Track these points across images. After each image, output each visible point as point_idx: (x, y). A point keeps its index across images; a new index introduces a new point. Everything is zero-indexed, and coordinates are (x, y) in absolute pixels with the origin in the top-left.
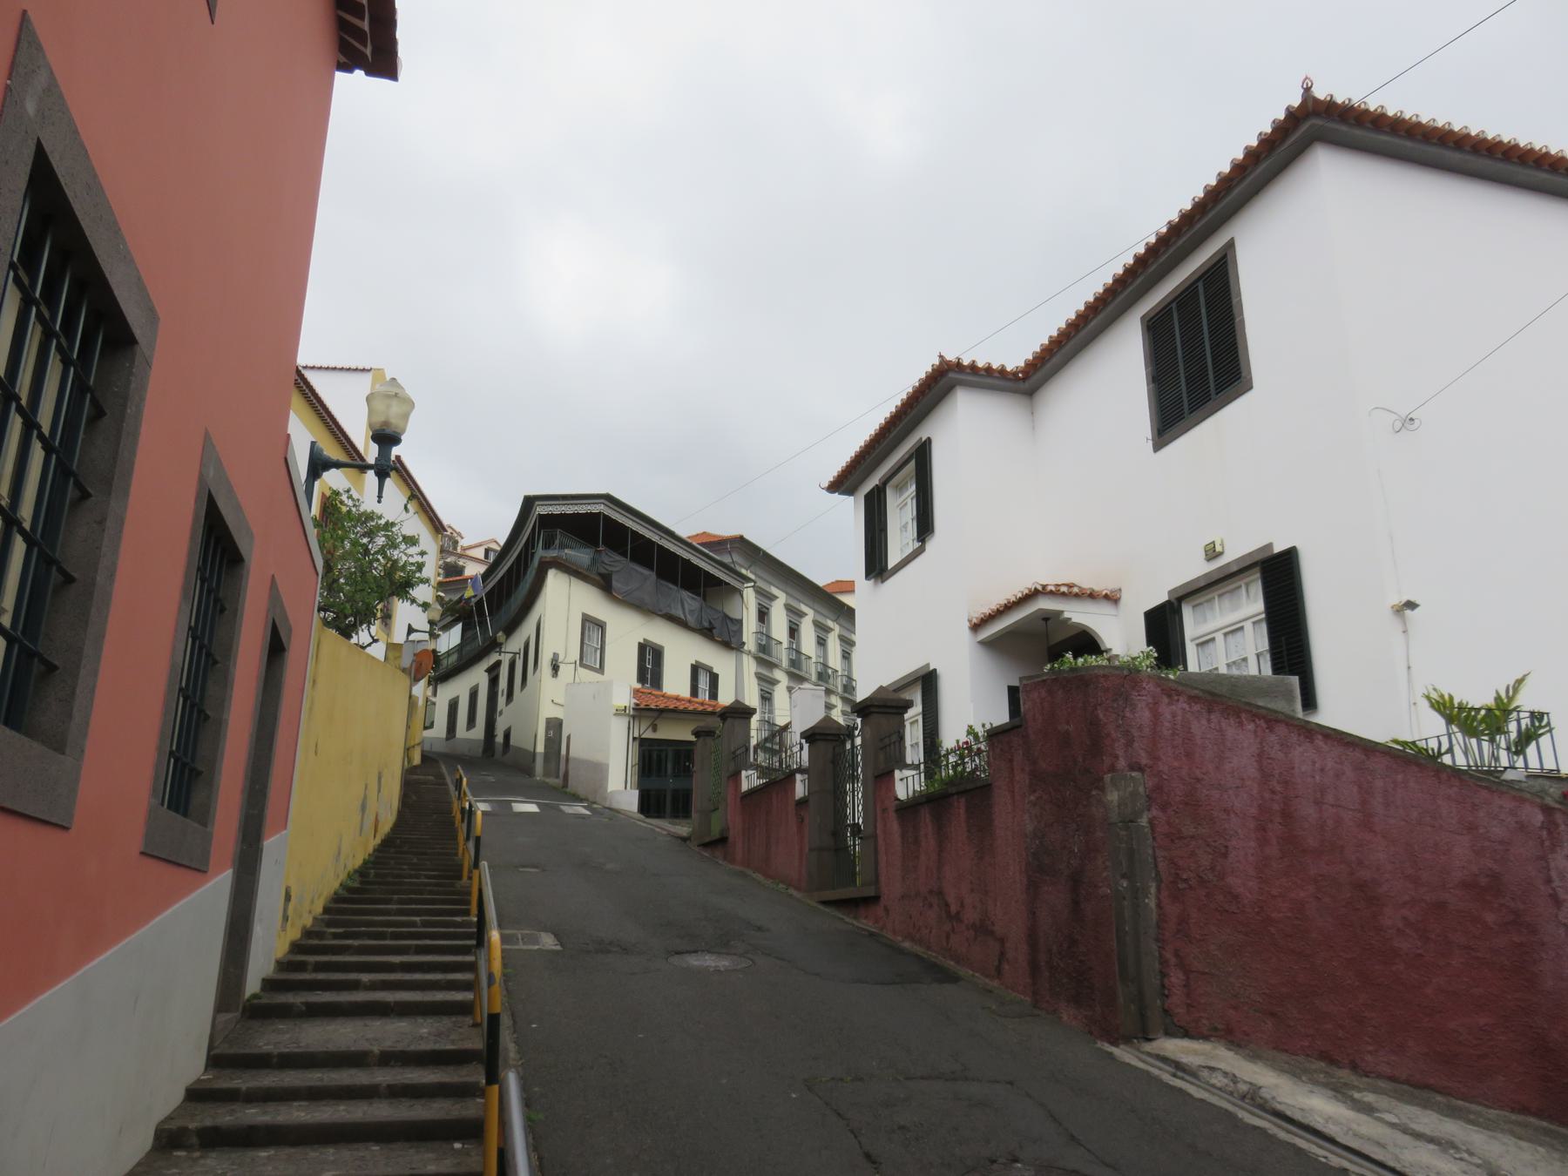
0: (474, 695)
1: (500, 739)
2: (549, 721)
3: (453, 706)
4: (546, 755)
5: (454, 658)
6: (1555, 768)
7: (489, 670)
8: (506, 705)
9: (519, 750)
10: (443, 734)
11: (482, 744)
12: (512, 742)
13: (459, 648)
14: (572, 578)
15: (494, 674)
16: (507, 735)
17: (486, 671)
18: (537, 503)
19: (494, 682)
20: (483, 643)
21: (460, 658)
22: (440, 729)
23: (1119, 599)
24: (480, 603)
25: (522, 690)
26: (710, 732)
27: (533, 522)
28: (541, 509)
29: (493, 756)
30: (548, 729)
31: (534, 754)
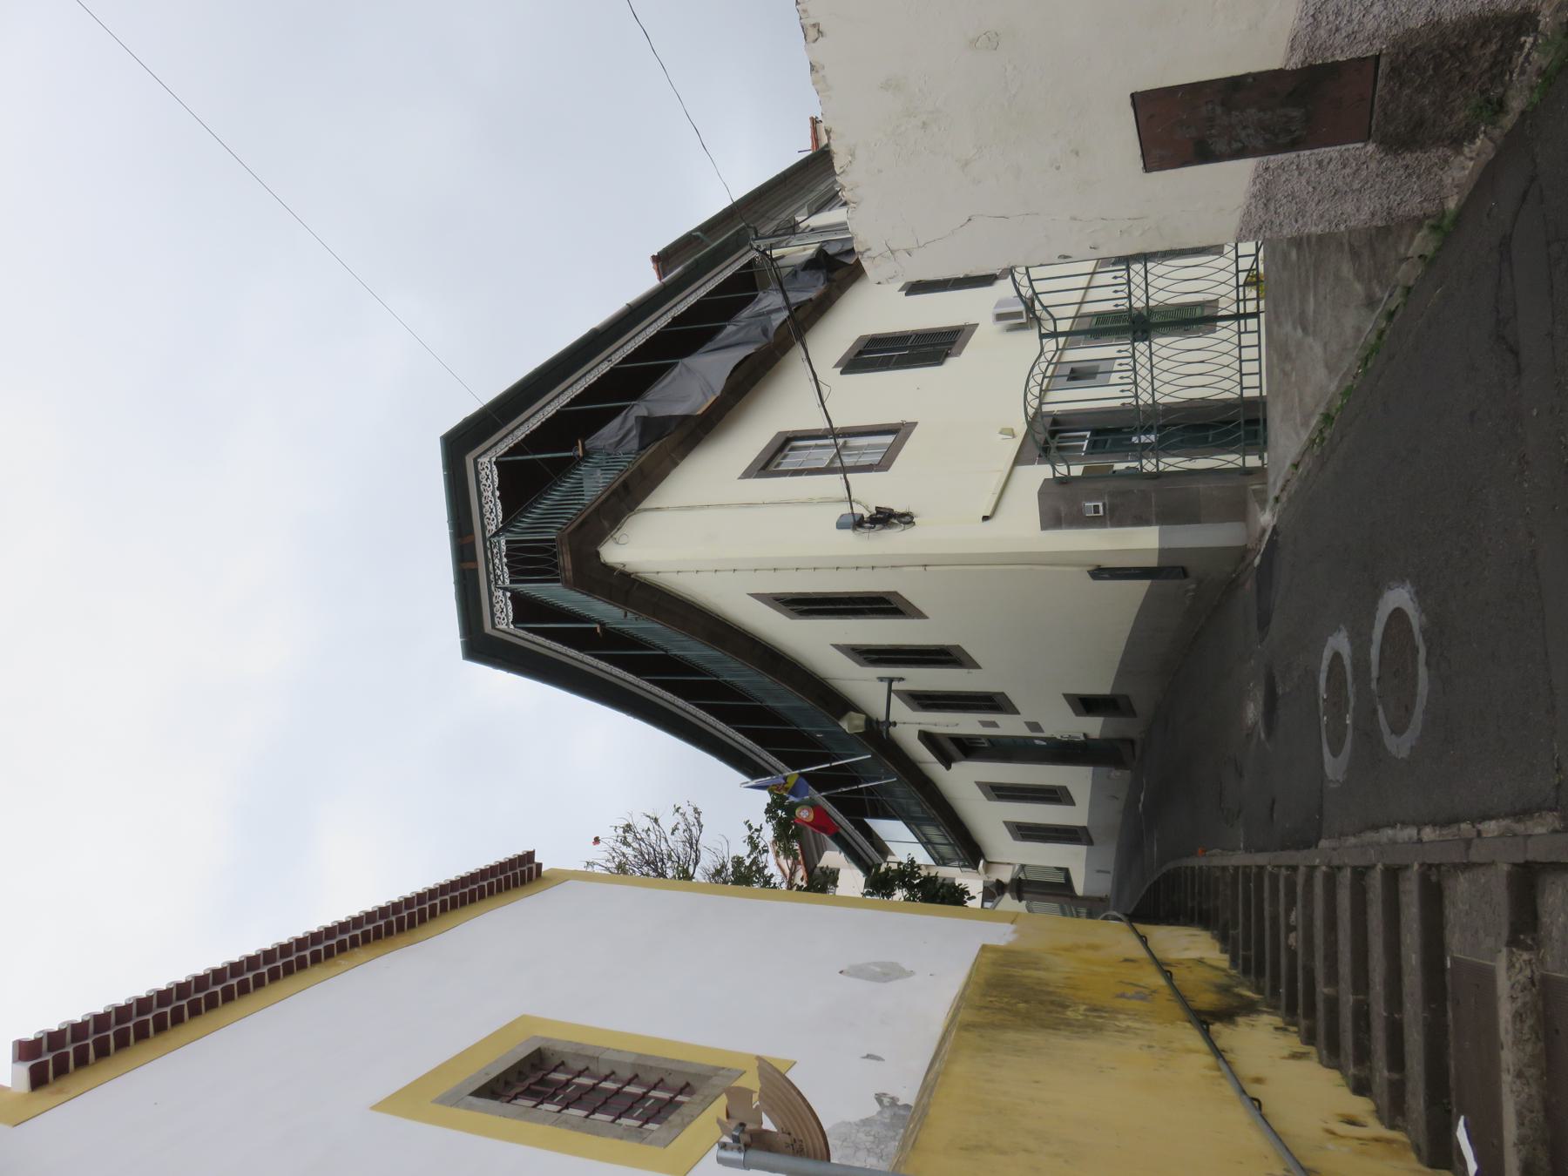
1: (1093, 726)
2: (1053, 518)
3: (1025, 832)
4: (1167, 516)
5: (933, 832)
6: (1225, 1035)
7: (947, 761)
8: (1018, 713)
9: (1127, 668)
10: (1080, 850)
11: (1103, 770)
12: (1101, 686)
13: (912, 822)
14: (645, 504)
16: (1086, 705)
17: (948, 767)
18: (488, 628)
19: (968, 748)
21: (930, 821)
23: (1392, 589)
25: (917, 614)
27: (530, 636)
28: (502, 618)
29: (1132, 742)
30: (1079, 520)
31: (1164, 571)
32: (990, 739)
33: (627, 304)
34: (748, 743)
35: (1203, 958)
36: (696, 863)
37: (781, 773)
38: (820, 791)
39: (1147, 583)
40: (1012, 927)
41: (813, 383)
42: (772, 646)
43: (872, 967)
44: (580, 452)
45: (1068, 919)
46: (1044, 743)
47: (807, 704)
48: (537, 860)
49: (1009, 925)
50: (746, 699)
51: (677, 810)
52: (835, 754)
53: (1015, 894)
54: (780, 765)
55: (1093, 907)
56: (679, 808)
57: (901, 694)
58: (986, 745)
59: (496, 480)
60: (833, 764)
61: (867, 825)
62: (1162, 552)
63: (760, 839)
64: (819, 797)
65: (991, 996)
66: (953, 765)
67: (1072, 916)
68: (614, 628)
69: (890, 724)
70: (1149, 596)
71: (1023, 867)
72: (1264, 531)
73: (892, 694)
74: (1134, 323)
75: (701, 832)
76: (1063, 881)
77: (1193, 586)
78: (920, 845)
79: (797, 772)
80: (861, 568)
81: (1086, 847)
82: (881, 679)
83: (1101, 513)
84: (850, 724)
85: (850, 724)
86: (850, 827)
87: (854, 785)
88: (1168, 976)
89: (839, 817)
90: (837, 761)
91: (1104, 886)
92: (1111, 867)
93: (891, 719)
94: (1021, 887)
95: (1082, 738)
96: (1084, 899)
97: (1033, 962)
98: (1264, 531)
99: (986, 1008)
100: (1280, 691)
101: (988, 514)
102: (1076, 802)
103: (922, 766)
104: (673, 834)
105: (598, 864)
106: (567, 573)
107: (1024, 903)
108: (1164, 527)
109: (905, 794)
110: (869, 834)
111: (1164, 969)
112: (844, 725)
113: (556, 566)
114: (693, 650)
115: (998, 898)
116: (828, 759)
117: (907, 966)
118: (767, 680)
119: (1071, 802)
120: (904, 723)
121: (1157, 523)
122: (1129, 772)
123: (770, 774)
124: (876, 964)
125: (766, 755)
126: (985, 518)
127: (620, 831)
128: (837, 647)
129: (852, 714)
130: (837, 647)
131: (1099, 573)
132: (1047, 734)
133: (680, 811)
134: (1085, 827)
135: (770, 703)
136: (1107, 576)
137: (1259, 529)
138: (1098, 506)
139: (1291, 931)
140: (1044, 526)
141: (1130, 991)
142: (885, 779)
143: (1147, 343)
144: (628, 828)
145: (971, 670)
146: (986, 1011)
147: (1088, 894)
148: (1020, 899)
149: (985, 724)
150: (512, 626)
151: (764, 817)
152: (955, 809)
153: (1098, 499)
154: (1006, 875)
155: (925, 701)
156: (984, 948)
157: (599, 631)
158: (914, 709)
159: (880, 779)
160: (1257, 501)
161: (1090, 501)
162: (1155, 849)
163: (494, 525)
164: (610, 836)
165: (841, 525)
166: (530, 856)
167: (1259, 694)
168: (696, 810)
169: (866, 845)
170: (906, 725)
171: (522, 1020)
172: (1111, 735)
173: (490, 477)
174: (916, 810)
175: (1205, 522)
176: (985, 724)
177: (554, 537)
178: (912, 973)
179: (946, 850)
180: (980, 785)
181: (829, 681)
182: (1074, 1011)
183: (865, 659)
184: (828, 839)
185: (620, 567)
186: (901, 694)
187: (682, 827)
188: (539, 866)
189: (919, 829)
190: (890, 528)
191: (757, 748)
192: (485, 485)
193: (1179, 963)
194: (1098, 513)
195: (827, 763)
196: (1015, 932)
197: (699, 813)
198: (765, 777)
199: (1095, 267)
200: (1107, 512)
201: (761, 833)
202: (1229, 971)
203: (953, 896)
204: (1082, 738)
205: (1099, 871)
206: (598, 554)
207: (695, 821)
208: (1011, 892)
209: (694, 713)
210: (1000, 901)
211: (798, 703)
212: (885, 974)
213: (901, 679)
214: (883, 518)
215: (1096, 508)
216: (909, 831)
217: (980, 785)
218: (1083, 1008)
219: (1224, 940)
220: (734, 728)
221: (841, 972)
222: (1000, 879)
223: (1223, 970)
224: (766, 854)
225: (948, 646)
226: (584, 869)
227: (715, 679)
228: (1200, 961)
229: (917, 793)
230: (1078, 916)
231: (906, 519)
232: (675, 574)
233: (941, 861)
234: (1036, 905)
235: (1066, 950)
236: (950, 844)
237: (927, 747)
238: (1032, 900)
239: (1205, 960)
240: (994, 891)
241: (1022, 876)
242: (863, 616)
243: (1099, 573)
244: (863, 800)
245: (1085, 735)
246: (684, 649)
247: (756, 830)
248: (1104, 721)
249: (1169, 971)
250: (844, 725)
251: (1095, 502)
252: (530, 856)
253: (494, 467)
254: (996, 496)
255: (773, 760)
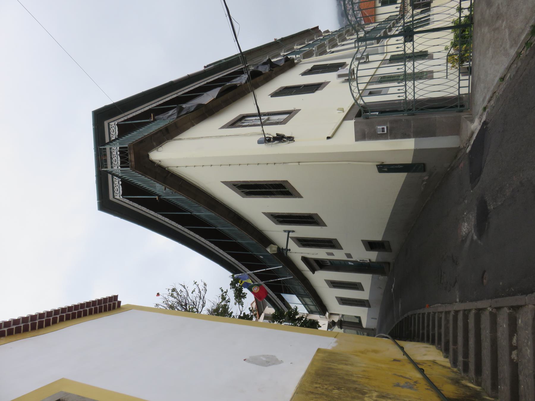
0: (335, 284)
1: (372, 256)
2: (361, 136)
3: (344, 301)
5: (308, 300)
7: (313, 270)
8: (342, 249)
10: (366, 309)
11: (376, 276)
12: (378, 237)
13: (299, 296)
15: (315, 265)
16: (371, 245)
17: (314, 273)
18: (111, 198)
20: (290, 275)
22: (361, 312)
24: (260, 276)
26: (381, 113)
27: (131, 203)
29: (389, 263)
32: (330, 260)
33: (188, 75)
34: (233, 259)
35: (435, 360)
36: (203, 306)
37: (246, 272)
38: (262, 281)
39: (405, 174)
40: (335, 340)
41: (228, 17)
42: (235, 211)
43: (262, 358)
44: (152, 120)
45: (359, 336)
46: (353, 264)
47: (254, 241)
48: (119, 299)
49: (334, 338)
50: (246, 251)
51: (195, 283)
52: (268, 265)
53: (339, 326)
54: (246, 270)
55: (370, 332)
56: (196, 282)
57: (293, 238)
58: (329, 264)
59: (117, 132)
60: (267, 269)
61: (282, 296)
62: (417, 152)
63: (226, 296)
64: (262, 283)
65: (316, 383)
66: (316, 272)
67: (361, 335)
68: (165, 199)
69: (287, 250)
70: (406, 185)
71: (343, 315)
72: (473, 133)
73: (289, 238)
74: (405, 32)
75: (205, 293)
76: (358, 322)
77: (426, 178)
78: (302, 305)
79: (252, 272)
80: (269, 164)
81: (367, 308)
82: (285, 231)
83: (386, 132)
84: (271, 250)
85: (271, 250)
86: (275, 297)
87: (276, 279)
88: (422, 371)
89: (268, 290)
90: (268, 268)
91: (374, 324)
92: (377, 316)
93: (288, 248)
94: (341, 324)
95: (368, 261)
96: (366, 329)
97: (345, 361)
98: (473, 133)
99: (312, 393)
100: (491, 207)
101: (330, 136)
102: (365, 290)
103: (303, 272)
104: (192, 293)
105: (160, 305)
106: (132, 163)
107: (343, 330)
108: (417, 139)
109: (299, 287)
110: (283, 300)
111: (415, 364)
112: (268, 250)
113: (127, 160)
114: (204, 213)
115: (333, 328)
116: (265, 267)
117: (279, 358)
118: (236, 229)
119: (362, 289)
120: (296, 253)
121: (414, 137)
122: (387, 277)
123: (241, 273)
124: (263, 356)
125: (240, 265)
126: (328, 138)
127: (170, 291)
128: (264, 213)
129: (272, 245)
130: (264, 213)
131: (383, 168)
132: (354, 259)
133: (197, 283)
134: (368, 300)
135: (240, 241)
136: (386, 169)
137: (469, 133)
138: (384, 128)
139: (514, 350)
140: (357, 139)
141: (402, 382)
142: (289, 277)
143: (412, 43)
144: (174, 290)
145: (322, 227)
146: (312, 396)
147: (368, 327)
148: (341, 329)
149: (329, 254)
150: (121, 197)
151: (230, 286)
152: (316, 290)
153: (384, 125)
154: (336, 319)
155: (304, 242)
156: (319, 350)
157: (157, 199)
158: (299, 247)
159: (287, 277)
160: (468, 120)
161: (380, 125)
162: (400, 307)
163: (115, 152)
164: (165, 293)
165: (260, 142)
166: (116, 297)
167: (472, 217)
168: (205, 285)
169: (280, 302)
170: (296, 254)
171: (62, 381)
172: (381, 260)
173: (114, 131)
174: (302, 291)
175: (439, 136)
176: (329, 254)
177: (127, 146)
178: (281, 362)
179: (313, 308)
180: (327, 281)
181: (263, 231)
182: (369, 397)
183: (277, 220)
184: (267, 301)
185: (157, 162)
186: (293, 238)
187: (197, 291)
188: (119, 303)
189: (303, 299)
190: (282, 142)
191: (236, 262)
192: (112, 135)
193: (424, 362)
194: (384, 132)
195: (278, 280)
196: (336, 342)
197: (206, 285)
198: (239, 274)
199: (380, 65)
200: (388, 131)
201: (227, 293)
202: (452, 368)
203: (314, 325)
204: (368, 261)
205: (372, 318)
206: (148, 156)
207: (204, 288)
208: (338, 325)
209: (214, 248)
210: (334, 328)
211: (251, 241)
212: (268, 362)
213: (293, 231)
214: (280, 138)
215: (383, 129)
216: (298, 299)
217: (327, 281)
218: (375, 394)
219: (446, 351)
220: (226, 253)
221: (245, 360)
222: (334, 320)
223: (449, 368)
224: (229, 303)
225: (312, 214)
226: (155, 307)
227: (215, 228)
228: (434, 362)
229: (301, 283)
230: (363, 335)
231: (291, 139)
232: (185, 168)
233: (311, 312)
234: (347, 330)
235: (362, 352)
236: (314, 305)
237: (305, 264)
238: (345, 329)
239: (437, 362)
240: (332, 325)
241: (342, 319)
242: (274, 196)
243: (383, 168)
244: (281, 285)
245: (370, 260)
246: (199, 211)
247: (225, 292)
248: (378, 254)
249: (422, 369)
250: (268, 250)
251: (382, 126)
252: (116, 297)
253: (116, 126)
254: (334, 130)
255: (243, 267)
